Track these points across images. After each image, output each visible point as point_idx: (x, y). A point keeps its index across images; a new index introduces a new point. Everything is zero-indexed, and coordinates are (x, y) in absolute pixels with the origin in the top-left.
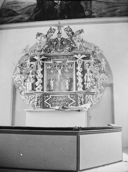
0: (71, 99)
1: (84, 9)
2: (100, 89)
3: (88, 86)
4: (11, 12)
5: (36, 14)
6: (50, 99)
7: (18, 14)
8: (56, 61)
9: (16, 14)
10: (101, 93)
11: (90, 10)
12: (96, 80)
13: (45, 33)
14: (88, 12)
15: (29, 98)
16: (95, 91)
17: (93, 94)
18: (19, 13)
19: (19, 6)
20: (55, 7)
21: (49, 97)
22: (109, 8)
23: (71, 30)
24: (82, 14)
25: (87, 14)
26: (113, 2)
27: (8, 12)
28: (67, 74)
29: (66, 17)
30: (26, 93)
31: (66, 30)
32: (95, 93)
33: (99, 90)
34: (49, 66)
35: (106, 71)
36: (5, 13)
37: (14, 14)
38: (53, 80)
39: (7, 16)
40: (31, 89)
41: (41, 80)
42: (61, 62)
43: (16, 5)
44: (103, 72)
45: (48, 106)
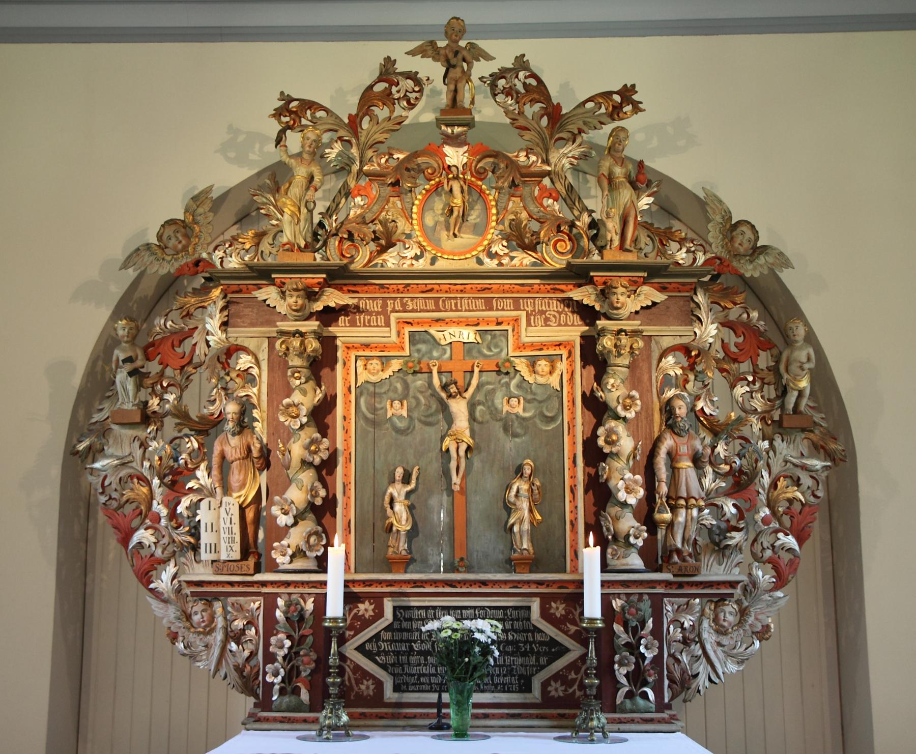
0: (550, 631)
2: (768, 553)
3: (685, 524)
6: (386, 629)
8: (432, 331)
10: (777, 586)
12: (740, 482)
15: (220, 622)
17: (723, 598)
21: (545, 685)
28: (515, 435)
30: (190, 583)
31: (502, 83)
33: (770, 561)
35: (817, 417)
38: (406, 480)
40: (230, 550)
41: (307, 477)
42: (468, 335)
44: (796, 421)
45: (367, 688)
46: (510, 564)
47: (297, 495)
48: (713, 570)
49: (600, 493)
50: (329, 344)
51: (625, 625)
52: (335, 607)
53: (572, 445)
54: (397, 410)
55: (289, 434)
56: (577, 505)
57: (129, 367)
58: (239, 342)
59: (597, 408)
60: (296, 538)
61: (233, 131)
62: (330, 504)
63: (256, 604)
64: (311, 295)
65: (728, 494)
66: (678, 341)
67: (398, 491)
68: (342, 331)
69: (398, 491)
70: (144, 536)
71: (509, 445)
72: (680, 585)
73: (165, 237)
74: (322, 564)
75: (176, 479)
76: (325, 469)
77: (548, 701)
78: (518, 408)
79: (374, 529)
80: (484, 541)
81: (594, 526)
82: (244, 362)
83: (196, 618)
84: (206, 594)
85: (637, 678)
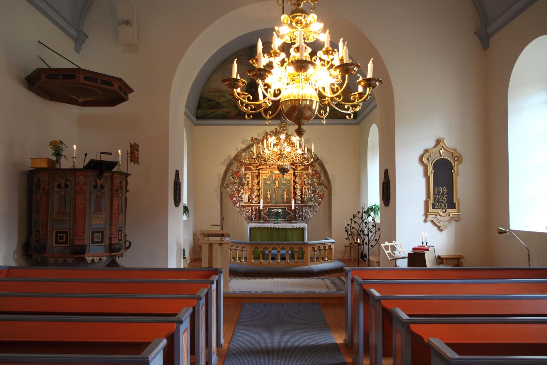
3: (306, 197)
9: (220, 106)
12: (314, 192)
27: (210, 103)
37: (218, 106)
39: (209, 108)
40: (247, 201)
41: (257, 191)
45: (265, 219)
46: (284, 203)
47: (255, 194)
48: (310, 203)
49: (295, 194)
50: (259, 173)
52: (261, 208)
53: (292, 187)
54: (268, 182)
55: (254, 186)
56: (292, 195)
59: (295, 182)
60: (255, 199)
61: (243, 139)
62: (260, 195)
63: (250, 208)
64: (257, 167)
67: (268, 193)
68: (261, 172)
69: (268, 193)
70: (234, 199)
71: (283, 187)
74: (259, 203)
75: (239, 191)
76: (259, 190)
77: (288, 220)
78: (285, 182)
79: (265, 199)
80: (280, 200)
81: (294, 198)
82: (247, 176)
84: (243, 206)
85: (299, 217)
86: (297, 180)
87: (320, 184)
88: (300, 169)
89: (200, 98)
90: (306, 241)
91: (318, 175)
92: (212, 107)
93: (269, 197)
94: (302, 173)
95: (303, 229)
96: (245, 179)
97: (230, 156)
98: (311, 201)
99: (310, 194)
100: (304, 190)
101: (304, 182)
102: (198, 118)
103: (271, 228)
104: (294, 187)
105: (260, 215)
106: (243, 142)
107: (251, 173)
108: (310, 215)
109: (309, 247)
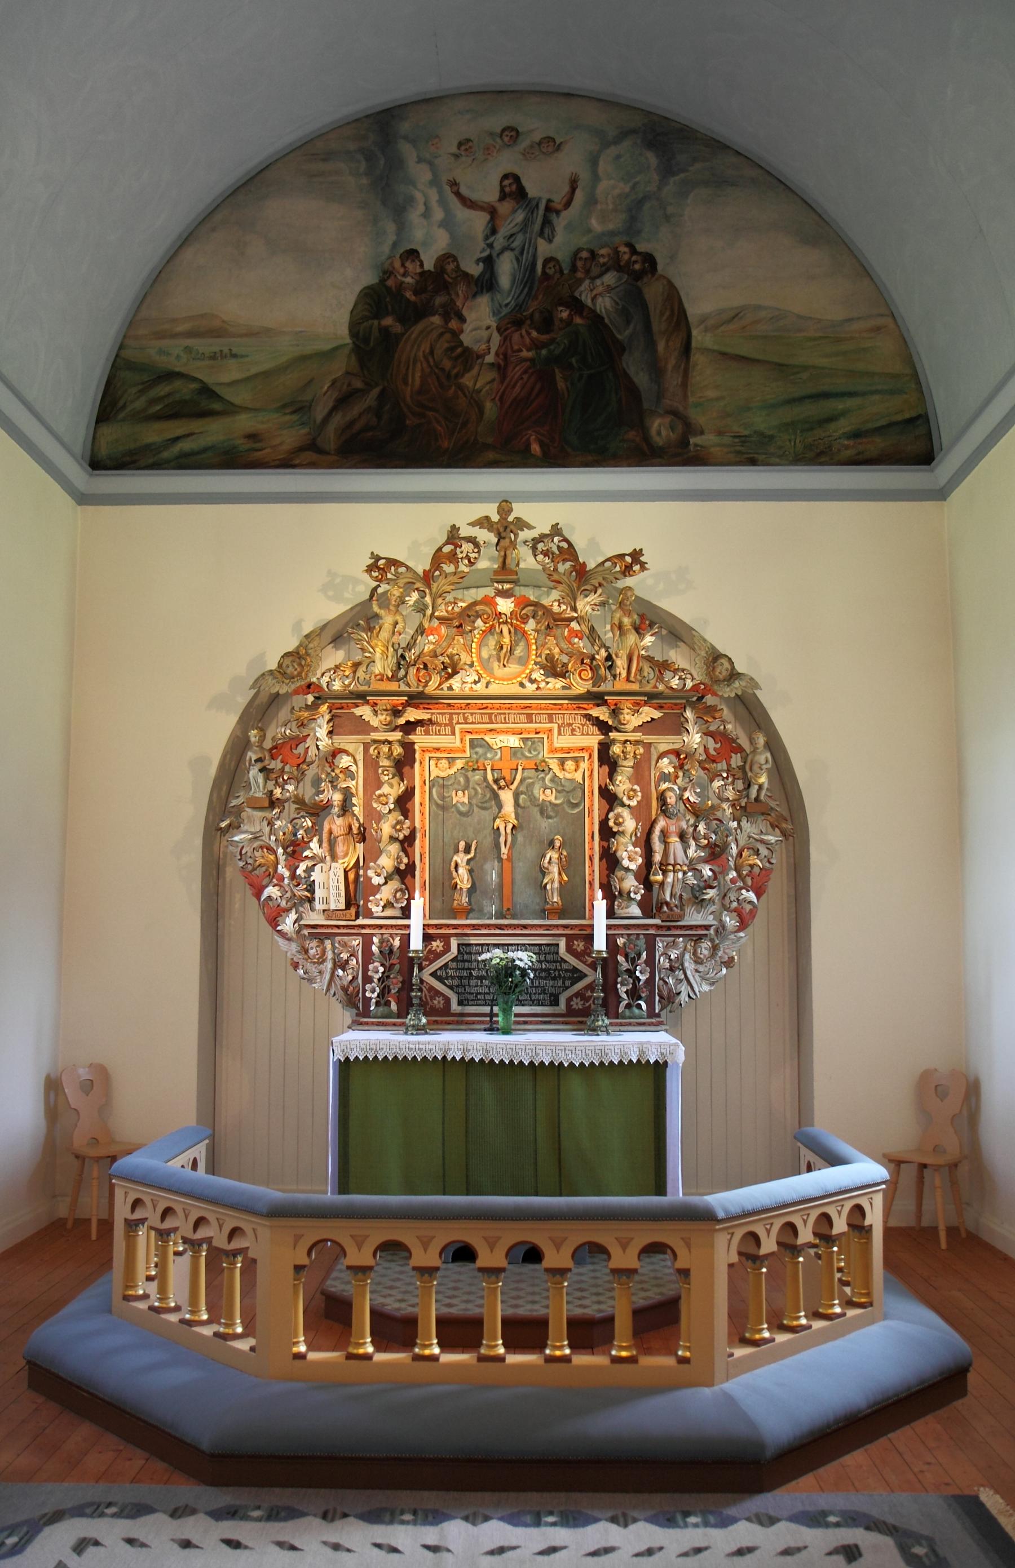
1: (646, 405)
2: (735, 904)
3: (671, 884)
4: (185, 390)
5: (348, 418)
6: (452, 960)
7: (231, 409)
8: (487, 738)
9: (217, 406)
11: (681, 409)
12: (715, 853)
13: (421, 566)
14: (668, 420)
15: (330, 955)
16: (710, 920)
17: (700, 938)
18: (239, 397)
19: (235, 350)
20: (467, 380)
22: (792, 401)
23: (569, 552)
24: (632, 434)
25: (659, 433)
26: (814, 367)
27: (162, 390)
28: (549, 817)
29: (536, 448)
31: (540, 546)
32: (712, 931)
34: (444, 763)
36: (142, 392)
37: (204, 402)
38: (467, 851)
39: (158, 417)
40: (337, 902)
41: (394, 848)
42: (514, 741)
43: (213, 345)
45: (438, 1002)
46: (543, 913)
47: (387, 862)
48: (694, 917)
49: (611, 861)
50: (409, 748)
51: (626, 956)
52: (416, 943)
53: (592, 825)
54: (460, 798)
55: (380, 817)
56: (594, 870)
57: (259, 765)
58: (341, 746)
59: (609, 798)
60: (386, 893)
62: (411, 868)
63: (356, 942)
64: (396, 713)
65: (706, 861)
66: (671, 747)
67: (461, 858)
68: (420, 739)
69: (461, 858)
71: (544, 825)
72: (669, 928)
73: (284, 665)
75: (295, 849)
76: (407, 843)
77: (570, 1012)
78: (550, 796)
79: (443, 888)
80: (525, 896)
82: (345, 761)
83: (312, 952)
84: (319, 934)
85: (634, 994)
86: (622, 784)
87: (744, 810)
88: (635, 721)
89: (115, 367)
90: (677, 1192)
91: (736, 760)
92: (177, 411)
93: (463, 878)
94: (648, 746)
95: (659, 1069)
96: (333, 782)
97: (261, 657)
98: (700, 903)
99: (692, 866)
100: (657, 846)
101: (662, 798)
102: (96, 464)
103: (467, 1065)
104: (604, 823)
105: (407, 985)
106: (331, 588)
107: (366, 747)
108: (696, 983)
109: (721, 1240)
